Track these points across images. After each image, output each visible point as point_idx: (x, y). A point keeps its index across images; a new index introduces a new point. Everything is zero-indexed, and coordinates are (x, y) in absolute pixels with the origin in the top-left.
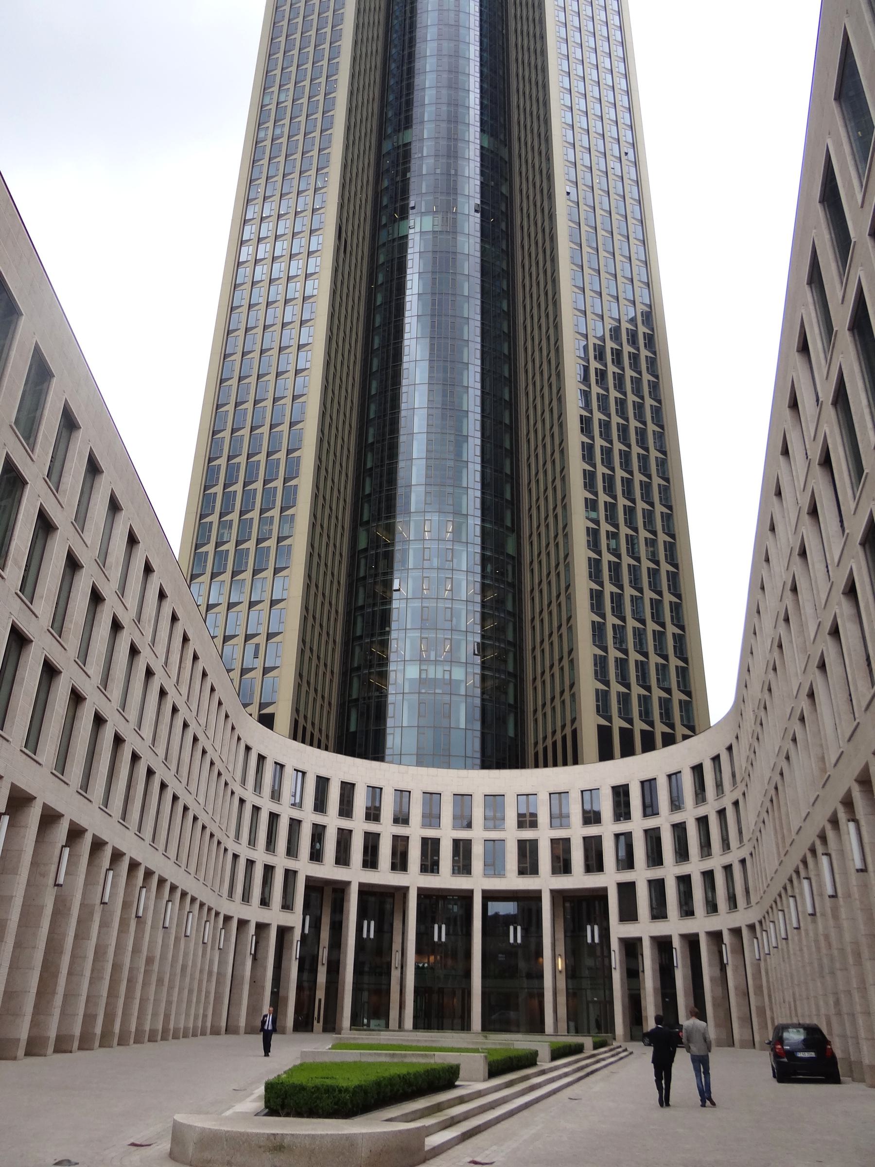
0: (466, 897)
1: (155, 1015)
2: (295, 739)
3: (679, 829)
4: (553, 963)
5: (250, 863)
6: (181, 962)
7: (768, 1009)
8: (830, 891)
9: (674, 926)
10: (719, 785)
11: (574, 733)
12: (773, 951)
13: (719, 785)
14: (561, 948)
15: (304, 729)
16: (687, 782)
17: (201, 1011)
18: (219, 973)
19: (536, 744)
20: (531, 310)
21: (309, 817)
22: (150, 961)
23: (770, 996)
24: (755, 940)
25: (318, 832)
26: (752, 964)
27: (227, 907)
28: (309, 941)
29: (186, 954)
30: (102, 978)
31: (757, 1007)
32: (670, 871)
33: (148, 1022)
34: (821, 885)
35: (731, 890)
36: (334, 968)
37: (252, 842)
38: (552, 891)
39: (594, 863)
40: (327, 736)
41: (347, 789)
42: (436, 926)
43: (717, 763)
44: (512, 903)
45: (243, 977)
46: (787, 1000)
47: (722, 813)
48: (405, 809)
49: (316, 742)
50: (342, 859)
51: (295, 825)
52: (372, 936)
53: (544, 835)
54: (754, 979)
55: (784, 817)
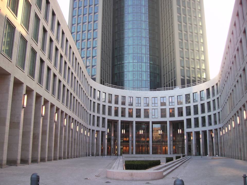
1: (83, 153)
2: (101, 84)
7: (223, 147)
11: (175, 81)
16: (205, 92)
18: (89, 143)
22: (75, 139)
26: (220, 137)
28: (109, 135)
31: (220, 147)
32: (200, 115)
35: (215, 120)
37: (94, 111)
39: (181, 114)
44: (159, 124)
47: (214, 100)
48: (131, 102)
50: (116, 114)
53: (167, 107)
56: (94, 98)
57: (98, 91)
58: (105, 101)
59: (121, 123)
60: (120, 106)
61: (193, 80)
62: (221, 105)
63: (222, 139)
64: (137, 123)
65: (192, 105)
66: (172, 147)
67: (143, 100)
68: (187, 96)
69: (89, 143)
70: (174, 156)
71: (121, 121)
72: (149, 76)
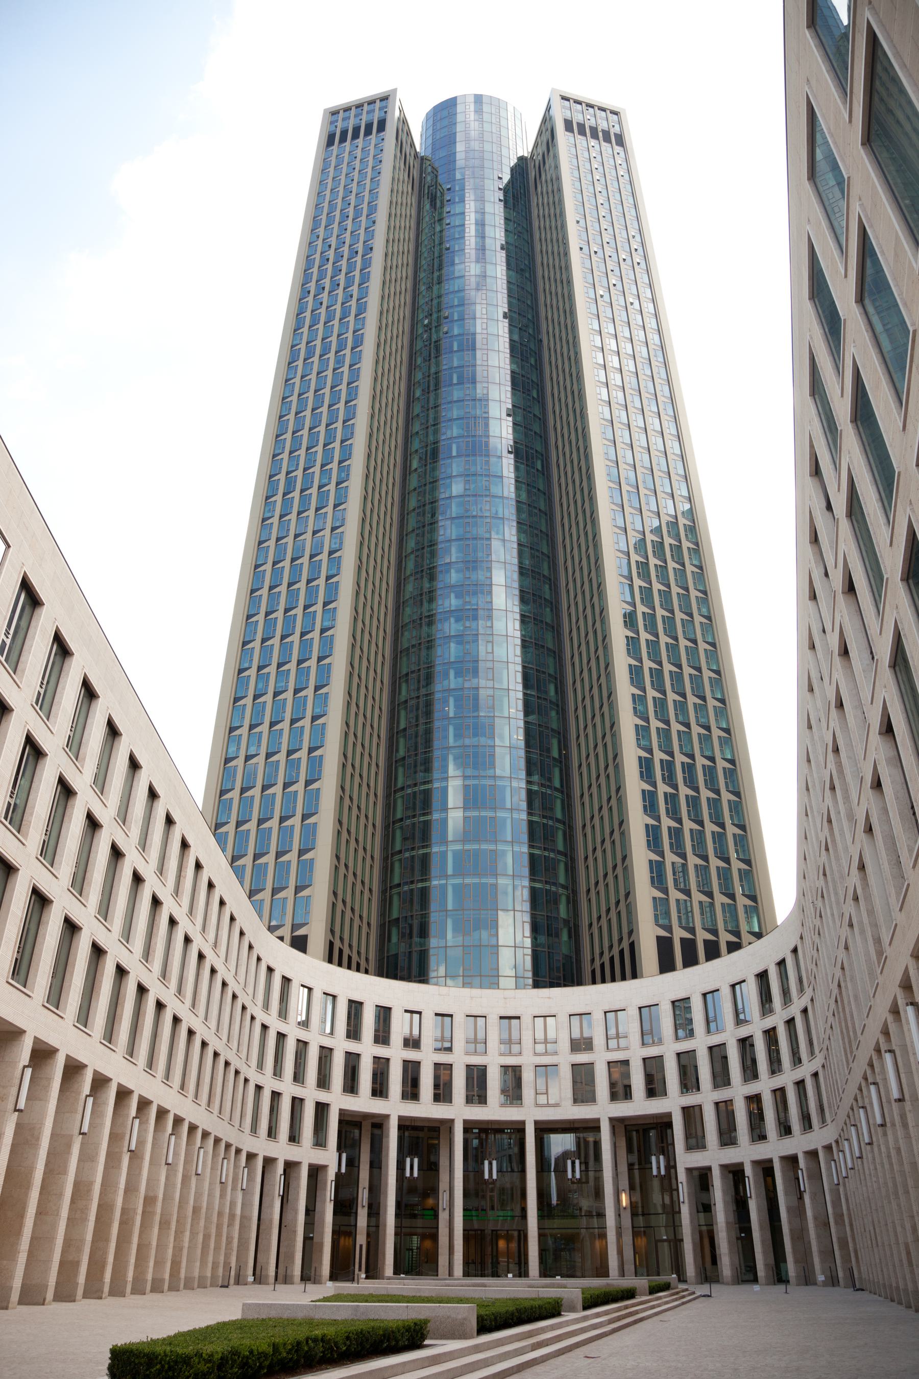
0: (518, 1129)
1: (159, 1263)
2: (330, 961)
3: (745, 1044)
4: (615, 1200)
5: (276, 1095)
6: (191, 1202)
7: (850, 1240)
8: (895, 1094)
9: (746, 1152)
10: (786, 992)
11: (632, 946)
12: (851, 1173)
13: (786, 992)
14: (624, 1182)
15: (341, 951)
16: (751, 990)
17: (222, 1258)
19: (593, 960)
20: (574, 496)
21: (341, 1045)
23: (851, 1225)
24: (833, 1163)
25: (352, 1060)
26: (831, 1190)
27: (249, 1144)
28: (346, 1181)
29: (198, 1195)
30: (85, 1219)
33: (151, 1270)
34: (888, 1091)
36: (375, 1211)
38: (611, 1119)
40: (367, 960)
41: (384, 1014)
42: (486, 1162)
43: (783, 965)
45: (271, 1221)
46: (867, 1230)
47: (790, 1022)
49: (354, 965)
50: (380, 1090)
51: (326, 1053)
52: (416, 1174)
53: (600, 1058)
54: (834, 1208)
55: (849, 1019)
56: (283, 1013)
57: (302, 986)
58: (305, 1024)
59: (401, 1127)
60: (396, 1054)
61: (705, 941)
62: (818, 1038)
63: (842, 1197)
64: (469, 1127)
65: (700, 1043)
66: (628, 1238)
67: (502, 1030)
68: (681, 1006)
69: (245, 1218)
70: (642, 1283)
71: (401, 1118)
72: (527, 927)
